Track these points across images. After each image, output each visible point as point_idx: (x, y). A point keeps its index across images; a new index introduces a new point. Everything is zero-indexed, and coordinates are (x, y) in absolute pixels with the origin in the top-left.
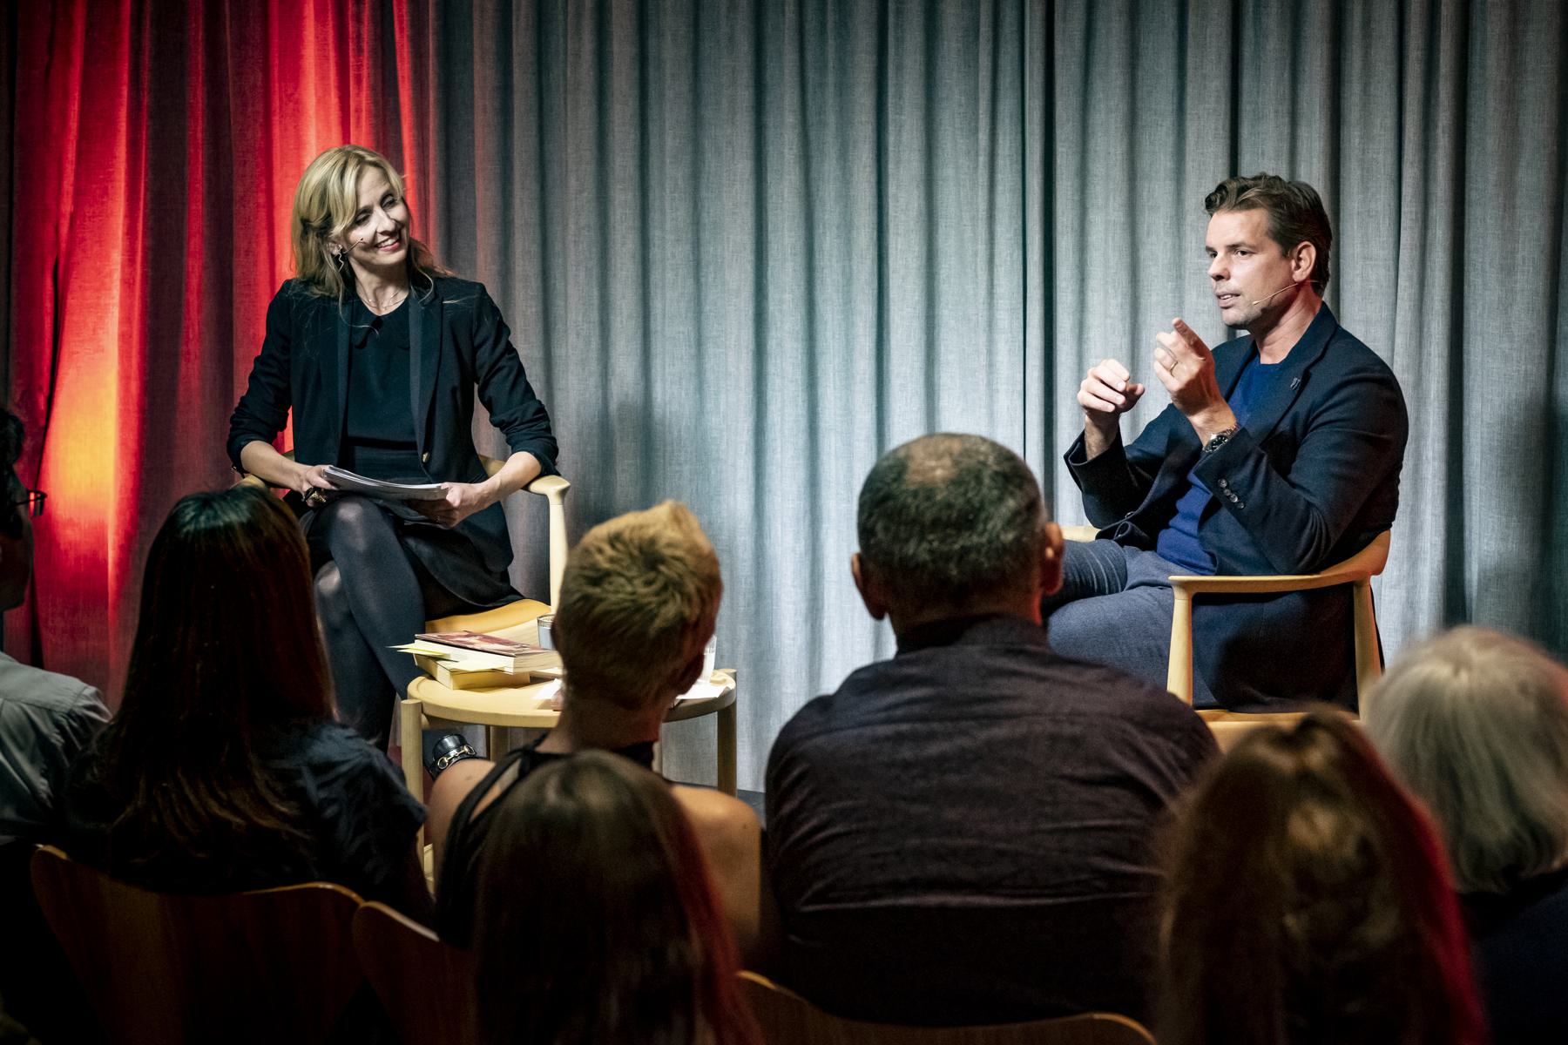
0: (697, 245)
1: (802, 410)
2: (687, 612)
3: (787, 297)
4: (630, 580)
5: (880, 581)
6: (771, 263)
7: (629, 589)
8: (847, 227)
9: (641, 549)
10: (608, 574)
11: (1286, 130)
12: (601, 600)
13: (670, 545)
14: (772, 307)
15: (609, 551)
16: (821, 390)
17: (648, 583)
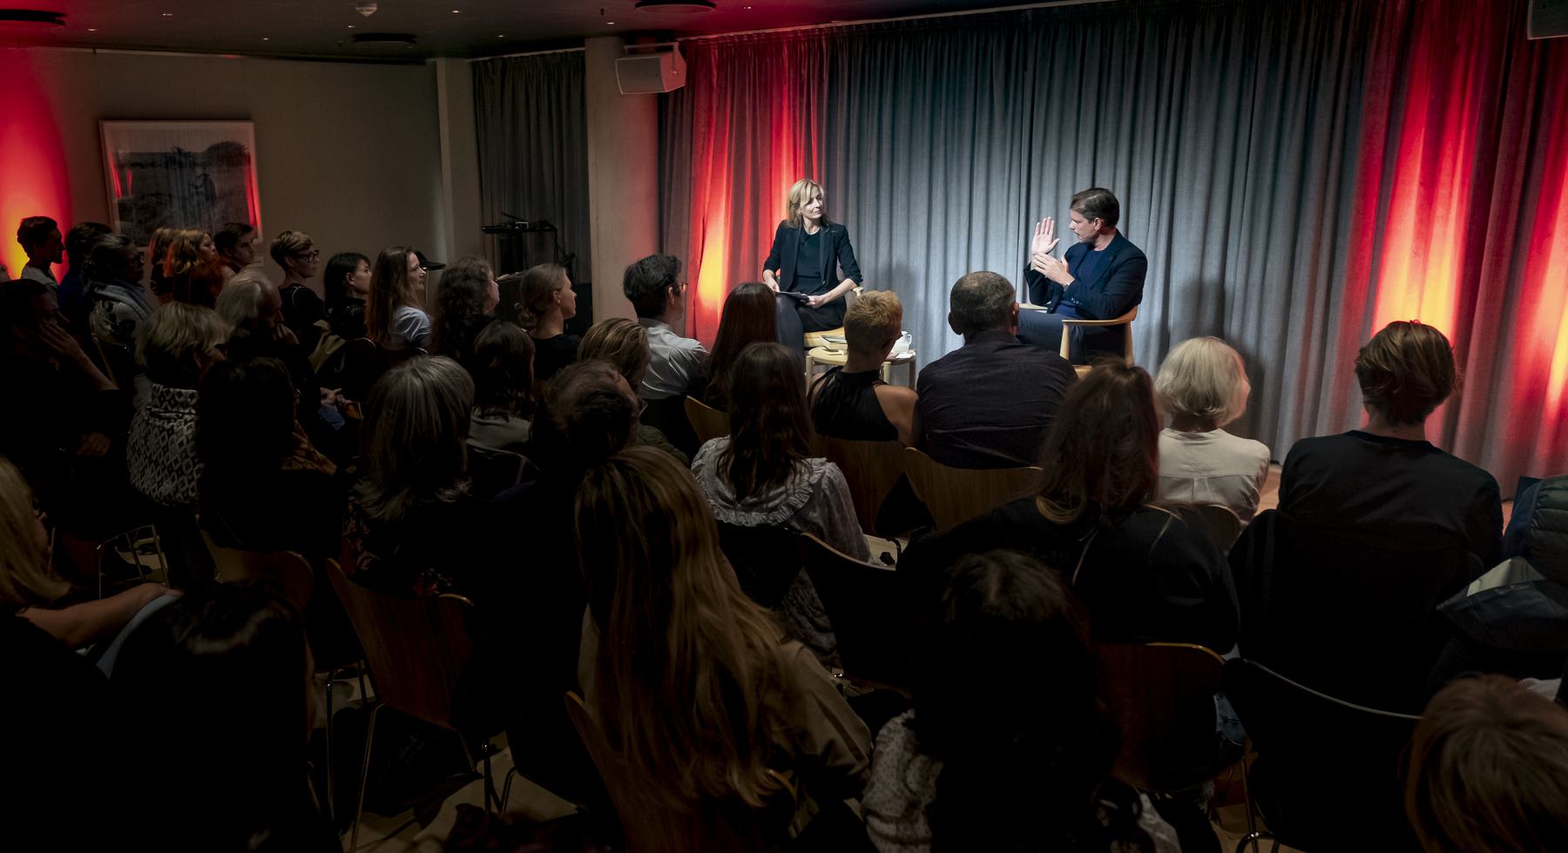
5: (959, 321)
8: (959, 205)
14: (933, 232)
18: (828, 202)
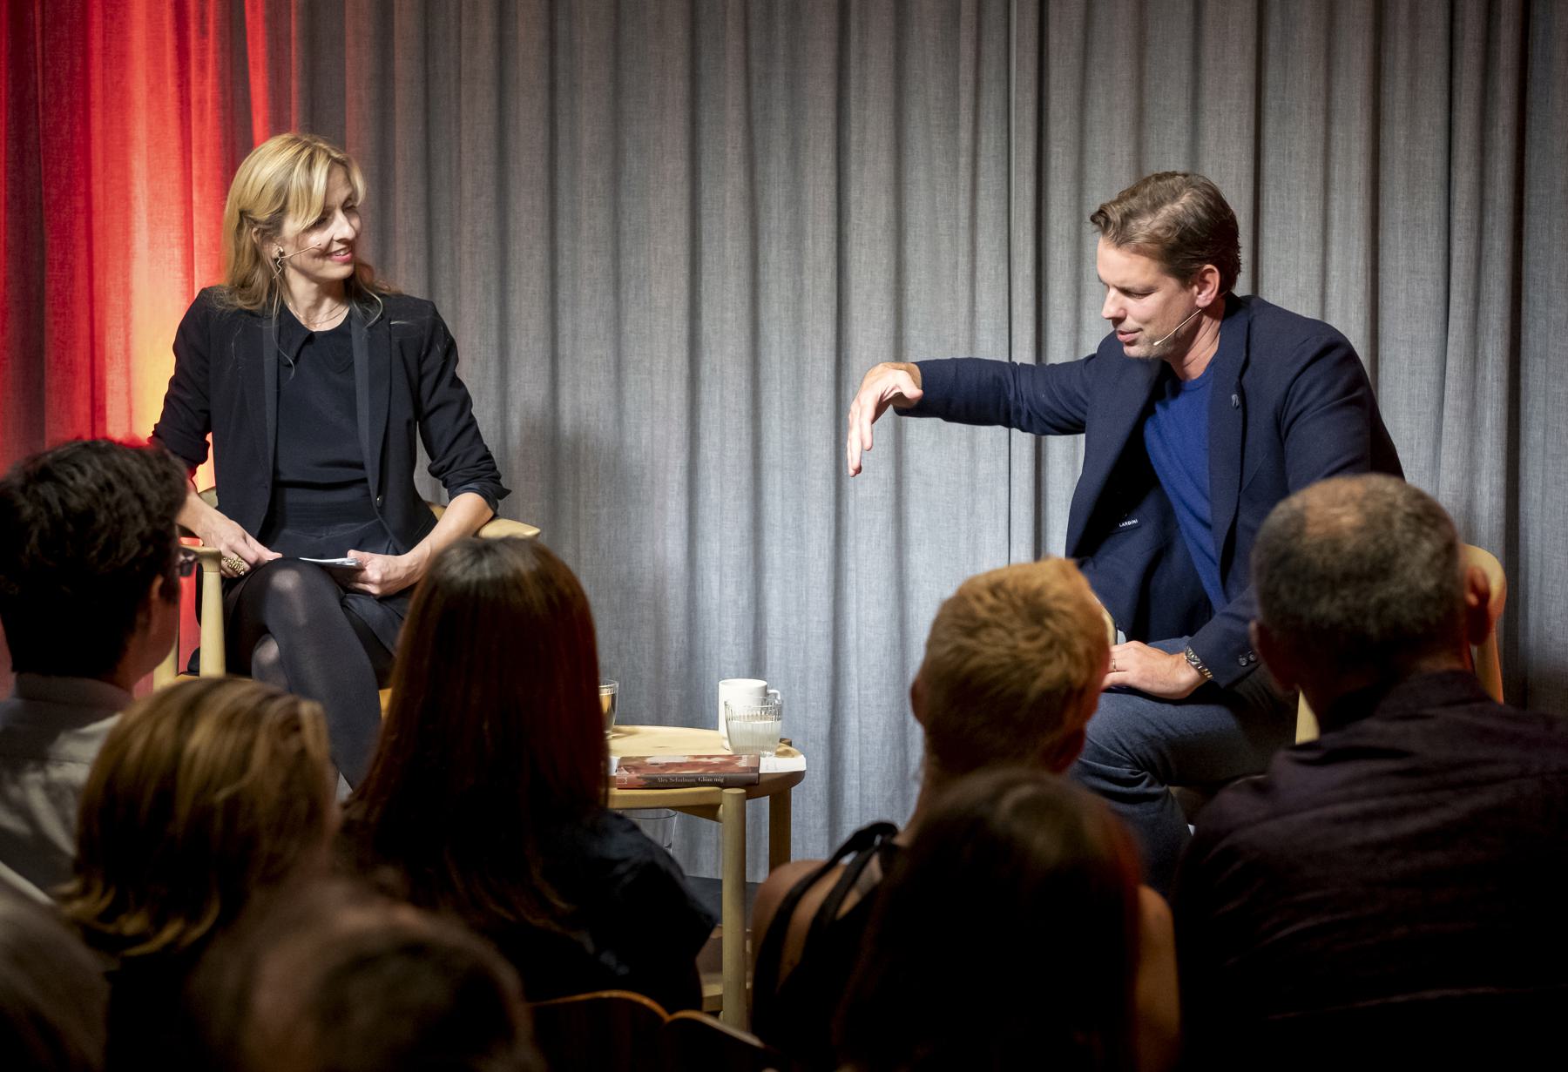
0: (616, 256)
1: (746, 444)
2: (1074, 673)
3: (729, 315)
4: (1011, 633)
6: (705, 277)
7: (1010, 642)
9: (1025, 599)
10: (985, 625)
11: (1320, 130)
12: (975, 653)
13: (1058, 598)
15: (989, 600)
16: (764, 422)
17: (1032, 638)
18: (378, 214)
